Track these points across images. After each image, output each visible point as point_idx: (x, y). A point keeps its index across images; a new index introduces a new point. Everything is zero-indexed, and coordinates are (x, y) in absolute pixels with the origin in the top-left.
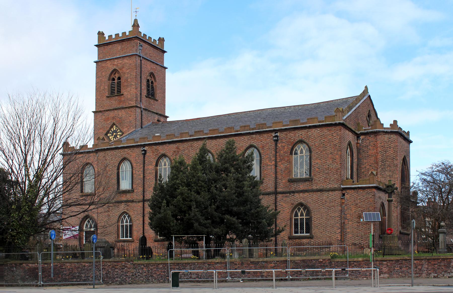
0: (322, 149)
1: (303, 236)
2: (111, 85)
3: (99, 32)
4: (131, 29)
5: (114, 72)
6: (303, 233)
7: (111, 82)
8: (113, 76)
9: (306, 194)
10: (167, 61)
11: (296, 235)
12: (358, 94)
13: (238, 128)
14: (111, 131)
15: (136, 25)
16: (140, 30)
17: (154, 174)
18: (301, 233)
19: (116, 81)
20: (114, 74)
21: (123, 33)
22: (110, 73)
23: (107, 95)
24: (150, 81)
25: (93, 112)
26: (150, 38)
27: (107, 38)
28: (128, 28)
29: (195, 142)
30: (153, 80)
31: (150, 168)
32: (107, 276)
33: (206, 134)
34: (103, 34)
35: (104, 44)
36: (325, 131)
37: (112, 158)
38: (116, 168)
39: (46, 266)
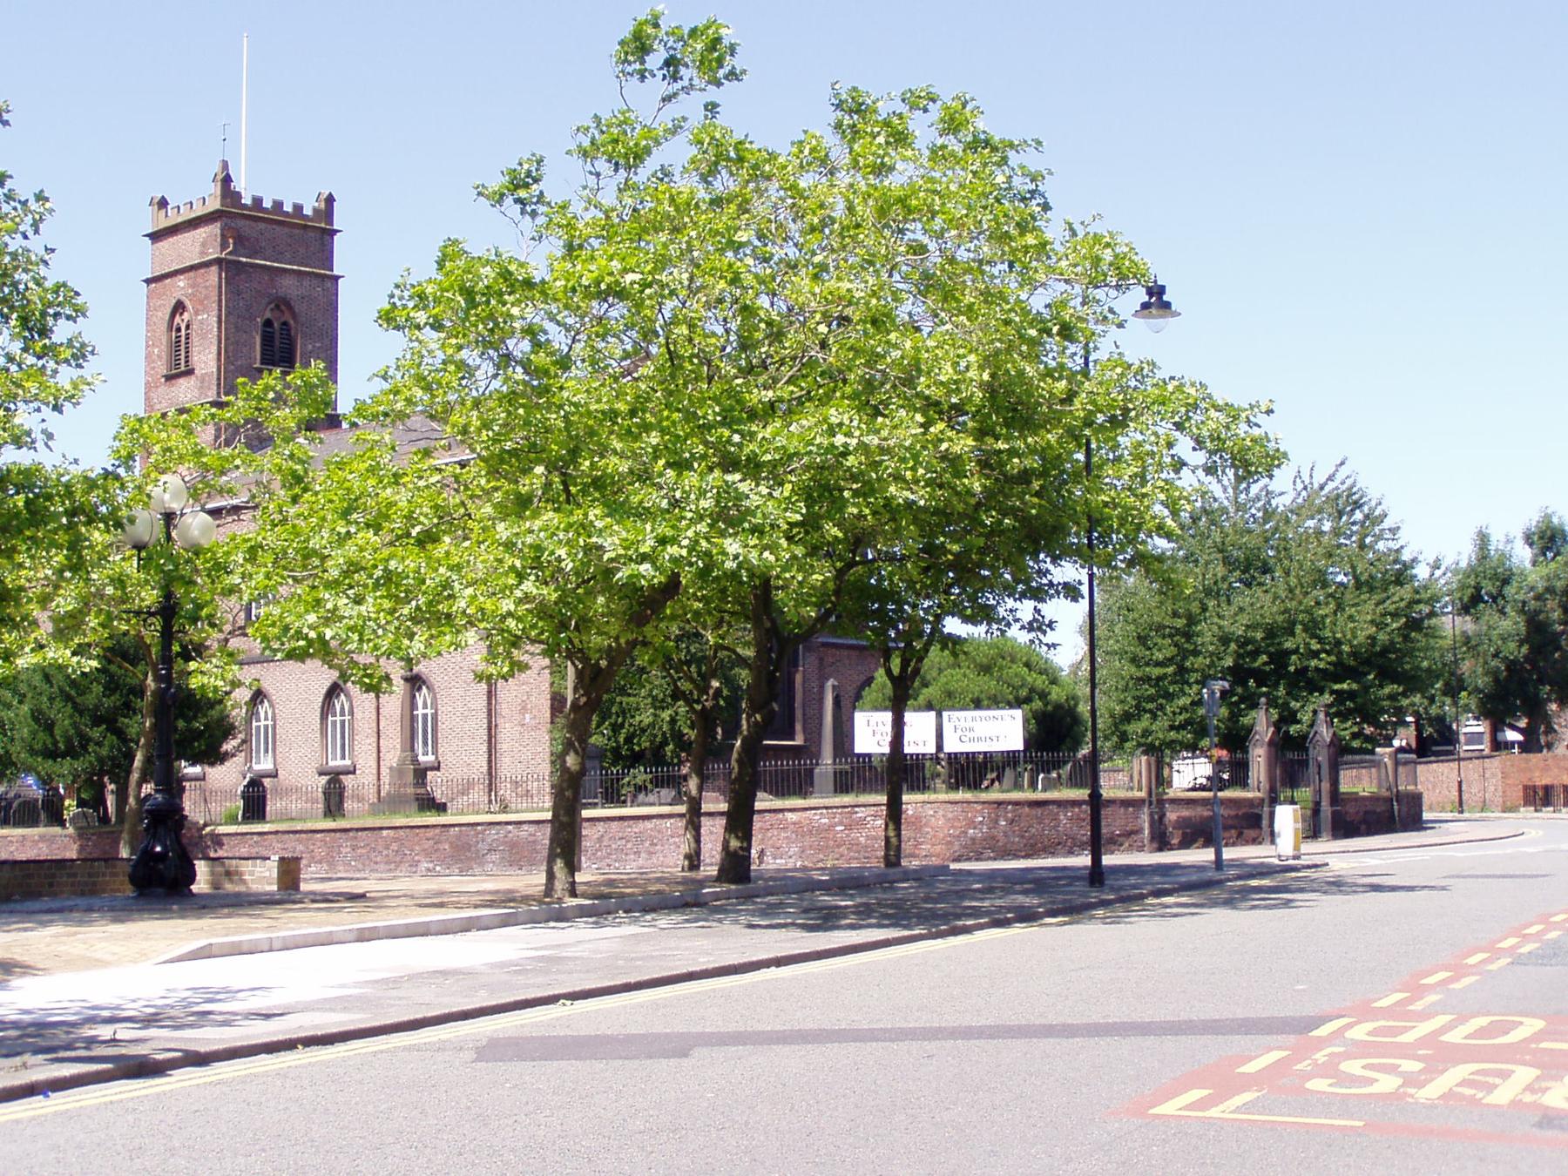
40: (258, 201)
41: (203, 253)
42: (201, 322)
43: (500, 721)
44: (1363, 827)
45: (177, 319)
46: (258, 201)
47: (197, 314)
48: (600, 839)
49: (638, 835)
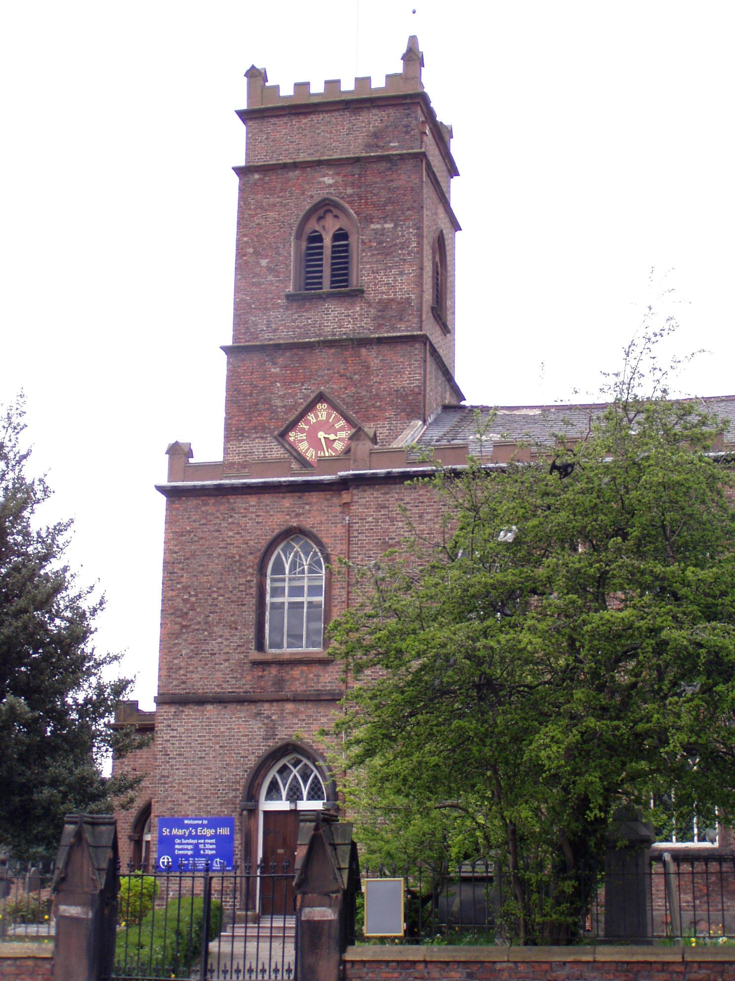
3: (253, 67)
5: (321, 212)
8: (313, 225)
14: (308, 422)
19: (328, 241)
20: (320, 219)
22: (302, 214)
23: (290, 289)
25: (224, 348)
26: (302, 87)
28: (380, 68)
41: (368, 146)
42: (383, 232)
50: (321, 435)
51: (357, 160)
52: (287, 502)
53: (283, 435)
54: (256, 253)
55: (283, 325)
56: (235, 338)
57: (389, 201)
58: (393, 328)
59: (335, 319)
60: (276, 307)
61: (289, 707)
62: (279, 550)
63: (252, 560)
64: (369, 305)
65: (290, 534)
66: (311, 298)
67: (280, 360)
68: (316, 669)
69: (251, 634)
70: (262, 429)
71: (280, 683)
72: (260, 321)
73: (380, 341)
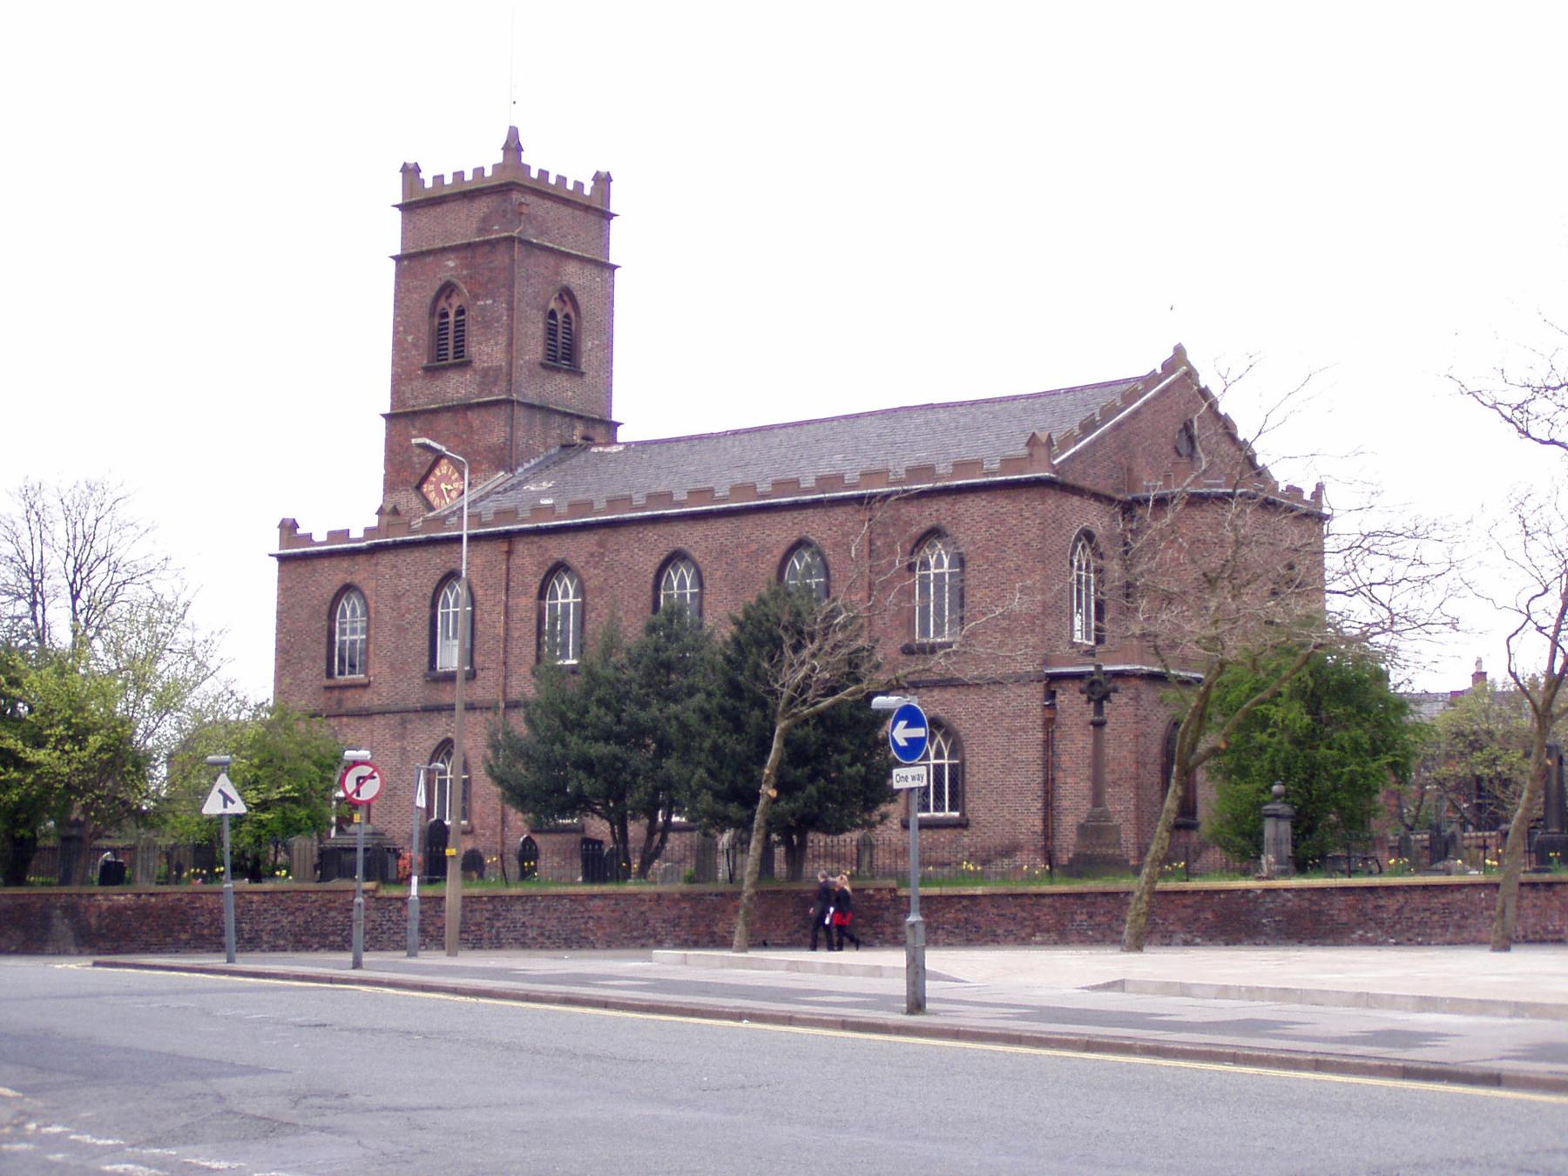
0: (992, 556)
1: (941, 819)
2: (436, 333)
4: (499, 157)
6: (943, 810)
7: (437, 321)
9: (948, 694)
10: (622, 244)
11: (940, 815)
12: (1143, 371)
13: (764, 487)
15: (513, 147)
16: (525, 159)
17: (534, 622)
18: (936, 809)
19: (452, 318)
21: (476, 171)
24: (560, 317)
27: (429, 184)
29: (650, 527)
30: (569, 309)
31: (525, 604)
32: (307, 929)
33: (680, 504)
34: (416, 169)
35: (421, 202)
36: (1003, 504)
37: (420, 571)
38: (428, 603)
39: (153, 900)
40: (544, 174)
41: (481, 231)
42: (484, 308)
43: (1060, 775)
44: (61, 926)
45: (443, 304)
46: (544, 174)
47: (476, 297)
48: (1399, 911)
49: (1446, 906)
50: (443, 486)
51: (469, 245)
52: (345, 563)
53: (419, 487)
54: (405, 332)
55: (426, 394)
56: (392, 407)
57: (490, 280)
58: (491, 393)
59: (456, 386)
60: (417, 376)
61: (345, 720)
62: (343, 601)
63: (325, 608)
64: (476, 372)
65: (347, 589)
66: (436, 369)
67: (418, 424)
68: (360, 691)
69: (323, 665)
70: (405, 483)
71: (340, 702)
72: (406, 390)
73: (479, 405)
